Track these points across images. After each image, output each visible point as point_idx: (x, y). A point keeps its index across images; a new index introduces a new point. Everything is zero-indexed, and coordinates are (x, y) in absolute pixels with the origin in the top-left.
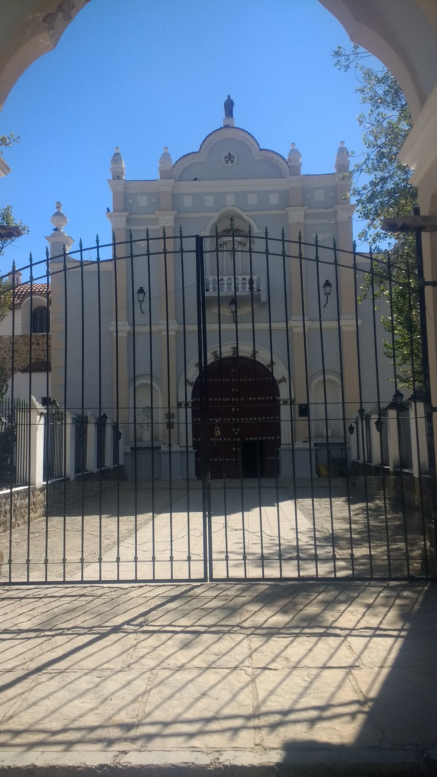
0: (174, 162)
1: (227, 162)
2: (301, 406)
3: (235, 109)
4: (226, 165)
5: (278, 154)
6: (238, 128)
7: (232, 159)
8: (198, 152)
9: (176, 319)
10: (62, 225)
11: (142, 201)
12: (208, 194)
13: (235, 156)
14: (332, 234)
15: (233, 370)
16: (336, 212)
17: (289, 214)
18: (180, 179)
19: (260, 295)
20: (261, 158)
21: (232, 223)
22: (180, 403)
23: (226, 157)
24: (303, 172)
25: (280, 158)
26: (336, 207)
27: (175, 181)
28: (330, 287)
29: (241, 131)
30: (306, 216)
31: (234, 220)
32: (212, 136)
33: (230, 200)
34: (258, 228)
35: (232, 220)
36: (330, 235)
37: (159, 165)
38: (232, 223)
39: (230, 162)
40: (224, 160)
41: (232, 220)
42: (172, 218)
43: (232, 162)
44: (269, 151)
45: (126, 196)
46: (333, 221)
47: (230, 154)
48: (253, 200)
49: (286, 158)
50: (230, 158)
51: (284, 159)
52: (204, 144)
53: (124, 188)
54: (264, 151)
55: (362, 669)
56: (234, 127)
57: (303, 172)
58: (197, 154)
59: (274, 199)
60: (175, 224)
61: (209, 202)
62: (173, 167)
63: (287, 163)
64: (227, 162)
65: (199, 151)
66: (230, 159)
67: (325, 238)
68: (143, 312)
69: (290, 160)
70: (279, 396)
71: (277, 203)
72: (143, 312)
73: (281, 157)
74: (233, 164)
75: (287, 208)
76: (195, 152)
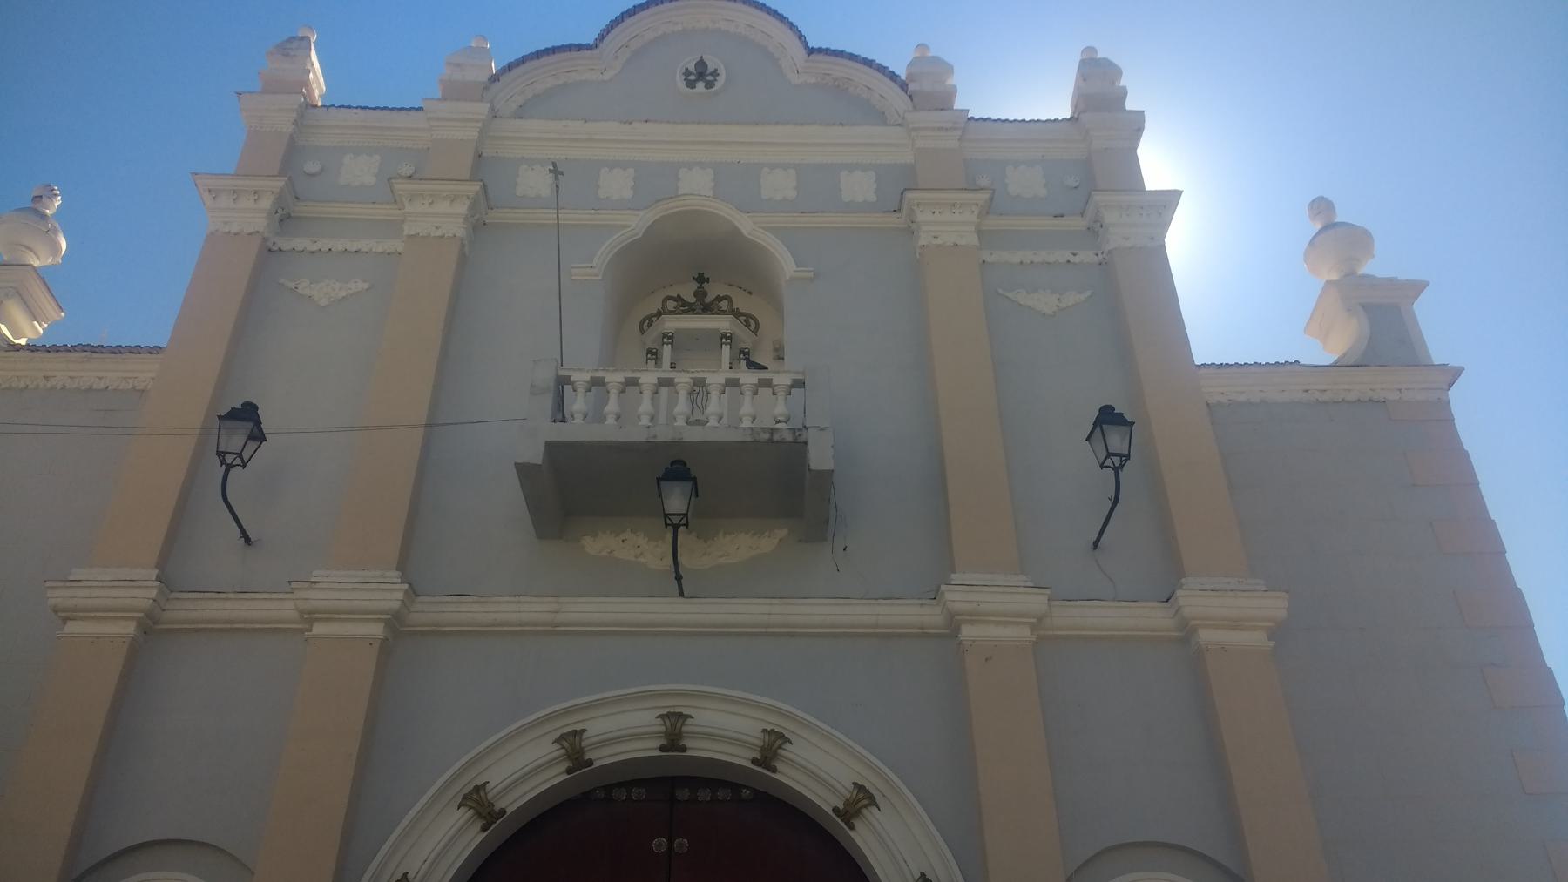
1: (691, 84)
5: (868, 63)
8: (588, 47)
10: (30, 249)
11: (360, 171)
12: (613, 165)
14: (1088, 293)
15: (660, 845)
19: (806, 443)
20: (813, 80)
23: (687, 73)
25: (880, 76)
28: (1125, 429)
33: (696, 189)
34: (796, 264)
36: (1082, 297)
39: (700, 86)
43: (710, 85)
47: (701, 64)
48: (779, 186)
49: (903, 77)
50: (701, 74)
51: (893, 76)
53: (295, 123)
54: (821, 57)
55: (295, 56)
59: (859, 187)
61: (617, 185)
63: (904, 86)
64: (691, 84)
68: (248, 540)
71: (872, 197)
73: (882, 69)
76: (580, 47)
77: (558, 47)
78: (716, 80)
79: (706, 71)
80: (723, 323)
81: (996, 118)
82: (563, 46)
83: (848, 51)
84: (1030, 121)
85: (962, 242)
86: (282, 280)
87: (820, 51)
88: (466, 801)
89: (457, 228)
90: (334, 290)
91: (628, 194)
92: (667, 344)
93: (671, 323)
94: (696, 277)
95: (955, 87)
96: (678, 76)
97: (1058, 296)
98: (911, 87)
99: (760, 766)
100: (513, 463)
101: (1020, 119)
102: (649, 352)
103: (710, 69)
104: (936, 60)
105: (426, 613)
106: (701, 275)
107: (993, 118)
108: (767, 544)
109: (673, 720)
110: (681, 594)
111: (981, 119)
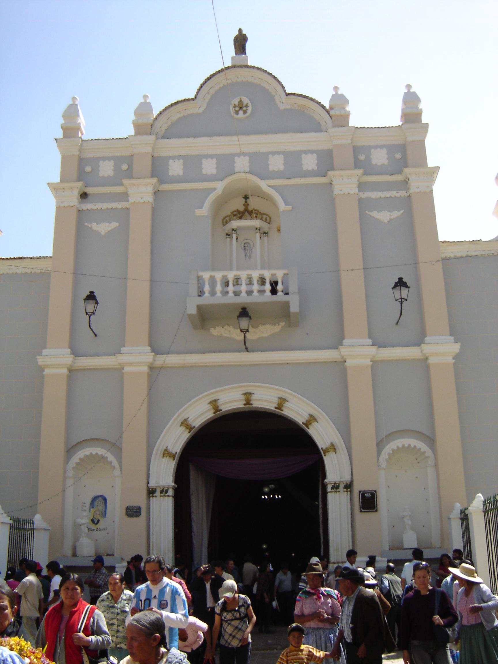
0: (155, 113)
1: (237, 113)
2: (363, 495)
3: (249, 46)
4: (236, 116)
6: (253, 67)
7: (245, 109)
8: (192, 99)
9: (370, 337)
13: (250, 105)
16: (406, 182)
17: (334, 183)
18: (166, 136)
20: (289, 107)
21: (246, 201)
22: (153, 489)
23: (235, 106)
24: (353, 122)
26: (407, 170)
27: (157, 138)
29: (258, 71)
30: (362, 186)
31: (249, 198)
32: (214, 78)
35: (246, 197)
37: (133, 117)
38: (246, 202)
39: (241, 112)
40: (232, 110)
41: (246, 197)
42: (150, 189)
43: (245, 112)
44: (301, 96)
45: (82, 161)
46: (402, 194)
47: (241, 102)
49: (328, 108)
51: (323, 107)
52: (202, 89)
54: (292, 97)
56: (247, 66)
57: (353, 122)
58: (192, 102)
60: (155, 200)
62: (156, 119)
63: (328, 112)
65: (196, 98)
66: (241, 108)
67: (392, 218)
69: (331, 108)
70: (324, 477)
71: (315, 168)
72: (96, 335)
73: (319, 103)
74: (246, 115)
75: (330, 173)
76: (189, 100)
77: (180, 101)
78: (247, 110)
79: (243, 105)
80: (256, 223)
81: (367, 127)
82: (182, 100)
83: (304, 94)
84: (381, 127)
85: (352, 192)
86: (86, 224)
87: (292, 94)
88: (182, 424)
89: (150, 198)
90: (106, 227)
91: (214, 171)
92: (234, 233)
93: (236, 223)
94: (244, 197)
95: (349, 111)
96: (231, 109)
97: (406, 191)
98: (332, 113)
99: (304, 425)
100: (376, 555)
101: (377, 127)
102: (227, 234)
103: (245, 104)
104: (342, 96)
105: (161, 360)
106: (246, 195)
107: (366, 127)
108: (277, 329)
109: (248, 395)
110: (248, 351)
111: (361, 128)
